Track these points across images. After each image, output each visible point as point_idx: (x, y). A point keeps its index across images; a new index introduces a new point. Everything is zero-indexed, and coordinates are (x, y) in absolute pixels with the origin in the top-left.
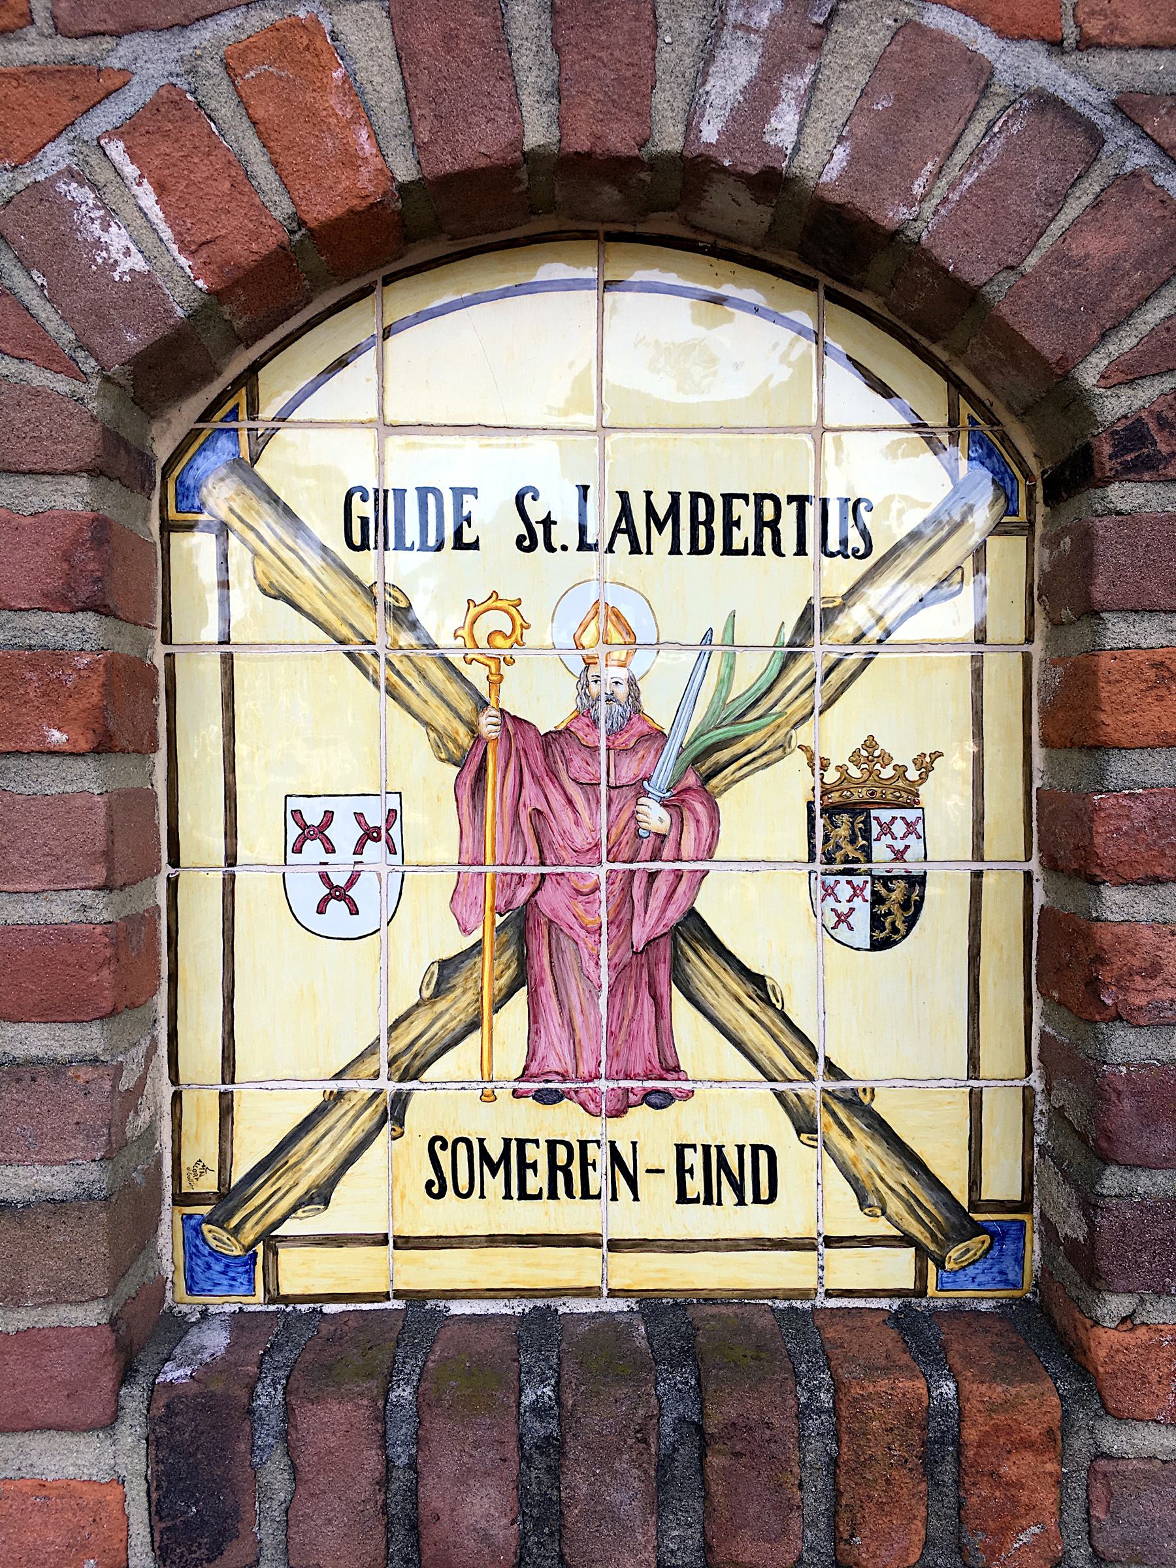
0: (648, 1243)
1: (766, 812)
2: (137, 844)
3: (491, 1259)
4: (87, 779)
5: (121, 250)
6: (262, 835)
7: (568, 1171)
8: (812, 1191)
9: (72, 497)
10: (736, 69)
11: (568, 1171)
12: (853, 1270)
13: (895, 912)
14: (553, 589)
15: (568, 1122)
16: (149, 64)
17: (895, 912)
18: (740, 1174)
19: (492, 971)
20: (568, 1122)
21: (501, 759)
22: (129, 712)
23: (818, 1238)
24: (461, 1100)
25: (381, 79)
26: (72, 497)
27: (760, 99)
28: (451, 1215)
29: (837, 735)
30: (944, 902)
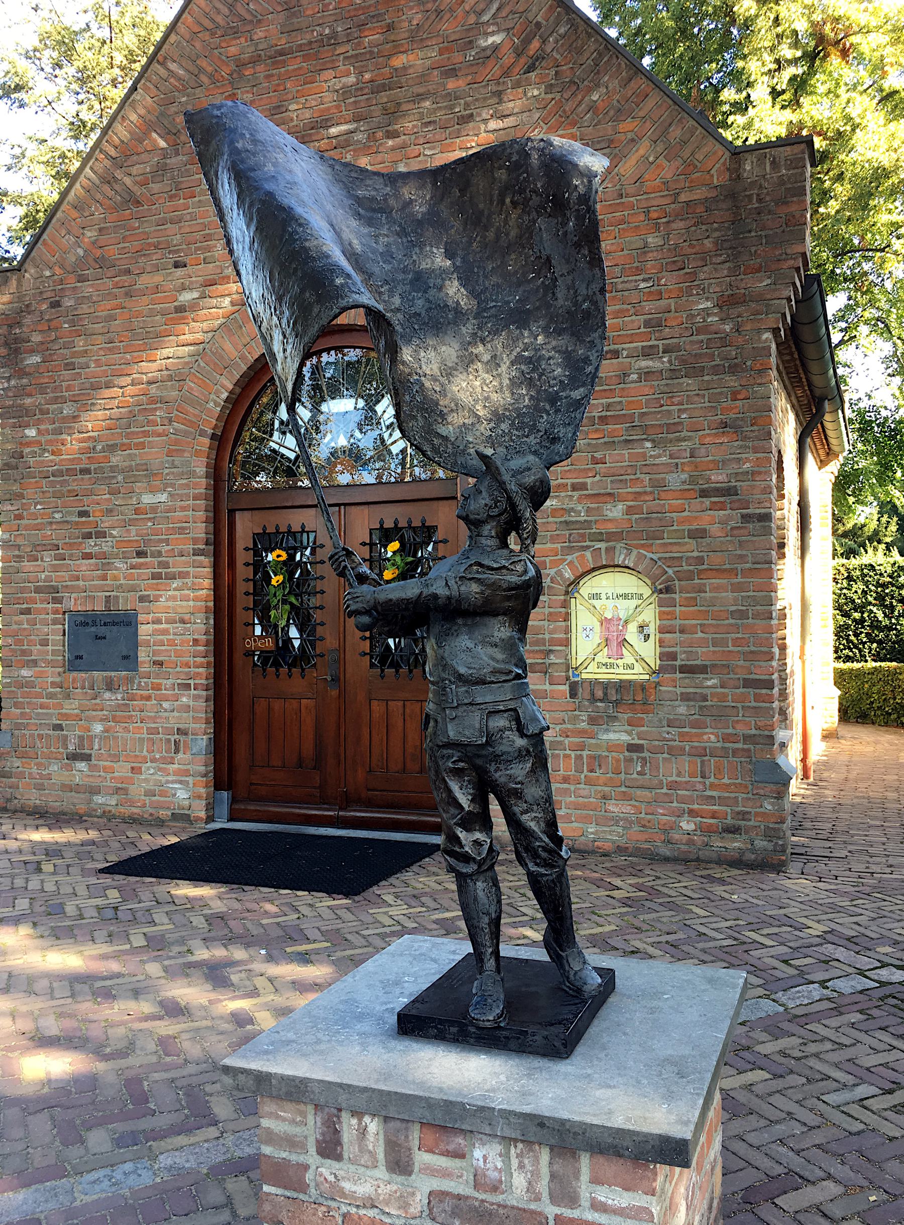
0: (620, 673)
1: (632, 628)
2: (568, 630)
3: (603, 675)
4: (563, 624)
5: (567, 576)
6: (580, 629)
7: (612, 665)
8: (638, 669)
9: (562, 597)
10: (622, 557)
11: (612, 665)
12: (642, 677)
13: (647, 638)
14: (610, 603)
15: (611, 661)
16: (569, 558)
17: (647, 638)
18: (632, 667)
19: (604, 644)
20: (611, 661)
21: (605, 622)
22: (567, 617)
23: (638, 674)
24: (602, 657)
25: (590, 559)
26: (562, 597)
27: (625, 559)
28: (625, 672)
29: (640, 619)
30: (652, 637)
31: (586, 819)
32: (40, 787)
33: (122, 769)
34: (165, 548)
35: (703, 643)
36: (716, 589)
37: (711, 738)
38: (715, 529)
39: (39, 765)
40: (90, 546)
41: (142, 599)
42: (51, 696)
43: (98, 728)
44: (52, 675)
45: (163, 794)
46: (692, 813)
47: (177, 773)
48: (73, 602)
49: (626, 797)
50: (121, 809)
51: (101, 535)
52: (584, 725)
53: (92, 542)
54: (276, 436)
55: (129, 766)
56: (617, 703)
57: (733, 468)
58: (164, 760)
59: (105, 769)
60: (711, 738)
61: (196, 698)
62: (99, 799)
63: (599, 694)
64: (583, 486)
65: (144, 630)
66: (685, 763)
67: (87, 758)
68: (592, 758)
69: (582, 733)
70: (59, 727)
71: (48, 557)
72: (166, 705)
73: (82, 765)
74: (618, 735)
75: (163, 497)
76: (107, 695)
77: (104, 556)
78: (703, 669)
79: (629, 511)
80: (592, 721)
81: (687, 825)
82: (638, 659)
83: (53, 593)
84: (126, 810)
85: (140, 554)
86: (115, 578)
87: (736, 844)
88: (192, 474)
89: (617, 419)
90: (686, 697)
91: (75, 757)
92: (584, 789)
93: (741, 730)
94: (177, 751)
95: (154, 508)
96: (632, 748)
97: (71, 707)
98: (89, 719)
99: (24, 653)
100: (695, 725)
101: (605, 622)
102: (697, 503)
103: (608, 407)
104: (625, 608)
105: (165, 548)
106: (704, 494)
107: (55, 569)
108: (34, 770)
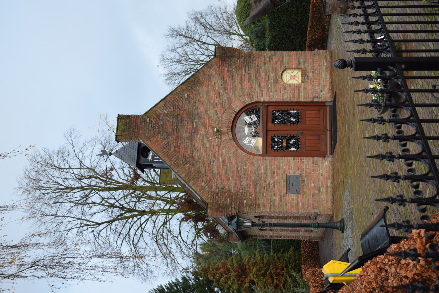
1: (292, 74)
3: (300, 79)
14: (288, 78)
21: (291, 79)
23: (300, 73)
31: (326, 81)
32: (327, 201)
33: (322, 178)
34: (273, 167)
35: (295, 62)
36: (286, 59)
37: (311, 60)
38: (276, 59)
39: (322, 201)
40: (272, 186)
41: (284, 173)
42: (306, 198)
43: (313, 185)
44: (301, 197)
45: (326, 168)
46: (323, 63)
47: (322, 165)
48: (284, 191)
49: (322, 74)
50: (331, 179)
51: (269, 183)
52: (309, 81)
53: (271, 185)
54: (251, 145)
55: (321, 177)
56: (305, 75)
57: (266, 57)
58: (319, 168)
59: (322, 183)
60: (311, 60)
61: (306, 160)
62: (329, 185)
63: (304, 78)
64: (267, 80)
65: (291, 172)
66: (315, 64)
67: (320, 188)
68: (315, 79)
69: (311, 81)
70: (313, 195)
71: (274, 198)
72: (307, 167)
73: (321, 189)
74: (311, 75)
75: (262, 167)
76: (305, 182)
77: (274, 182)
78: (299, 62)
79: (272, 73)
80: (308, 79)
81: (326, 64)
82: (298, 73)
83: (282, 196)
84: (331, 177)
85: (274, 173)
86: (279, 180)
87: (328, 57)
88: (258, 159)
89: (256, 74)
90: (304, 64)
91: (319, 191)
92: (321, 80)
93: (309, 56)
94: (317, 164)
95: (265, 169)
96: (313, 72)
97: (308, 192)
98: (311, 187)
99: (296, 205)
100: (309, 63)
101: (291, 79)
102: (271, 62)
103: (254, 76)
104: (288, 75)
105: (273, 167)
106: (270, 61)
107: (277, 196)
108: (323, 203)
